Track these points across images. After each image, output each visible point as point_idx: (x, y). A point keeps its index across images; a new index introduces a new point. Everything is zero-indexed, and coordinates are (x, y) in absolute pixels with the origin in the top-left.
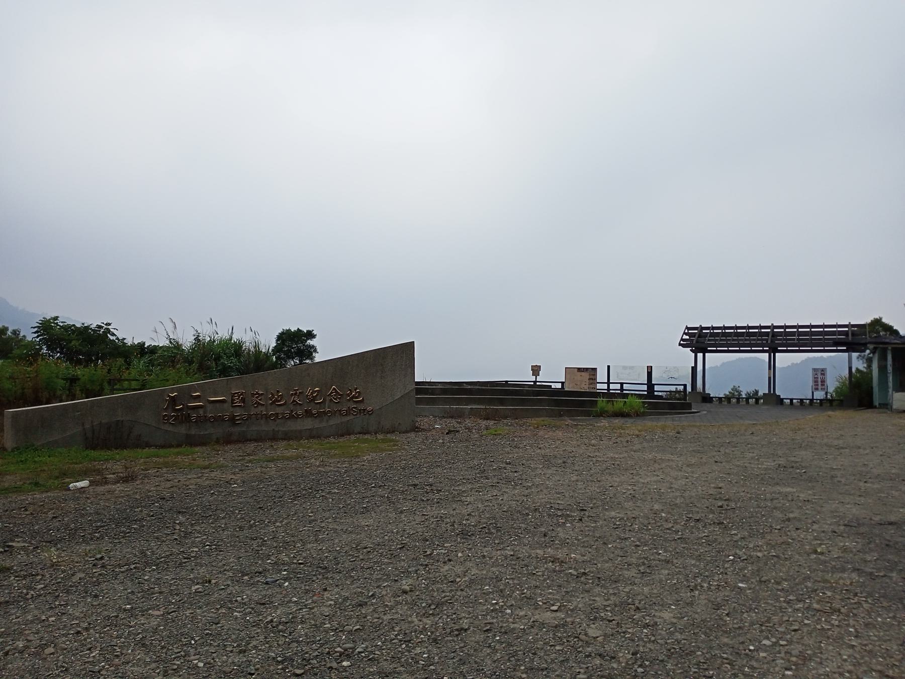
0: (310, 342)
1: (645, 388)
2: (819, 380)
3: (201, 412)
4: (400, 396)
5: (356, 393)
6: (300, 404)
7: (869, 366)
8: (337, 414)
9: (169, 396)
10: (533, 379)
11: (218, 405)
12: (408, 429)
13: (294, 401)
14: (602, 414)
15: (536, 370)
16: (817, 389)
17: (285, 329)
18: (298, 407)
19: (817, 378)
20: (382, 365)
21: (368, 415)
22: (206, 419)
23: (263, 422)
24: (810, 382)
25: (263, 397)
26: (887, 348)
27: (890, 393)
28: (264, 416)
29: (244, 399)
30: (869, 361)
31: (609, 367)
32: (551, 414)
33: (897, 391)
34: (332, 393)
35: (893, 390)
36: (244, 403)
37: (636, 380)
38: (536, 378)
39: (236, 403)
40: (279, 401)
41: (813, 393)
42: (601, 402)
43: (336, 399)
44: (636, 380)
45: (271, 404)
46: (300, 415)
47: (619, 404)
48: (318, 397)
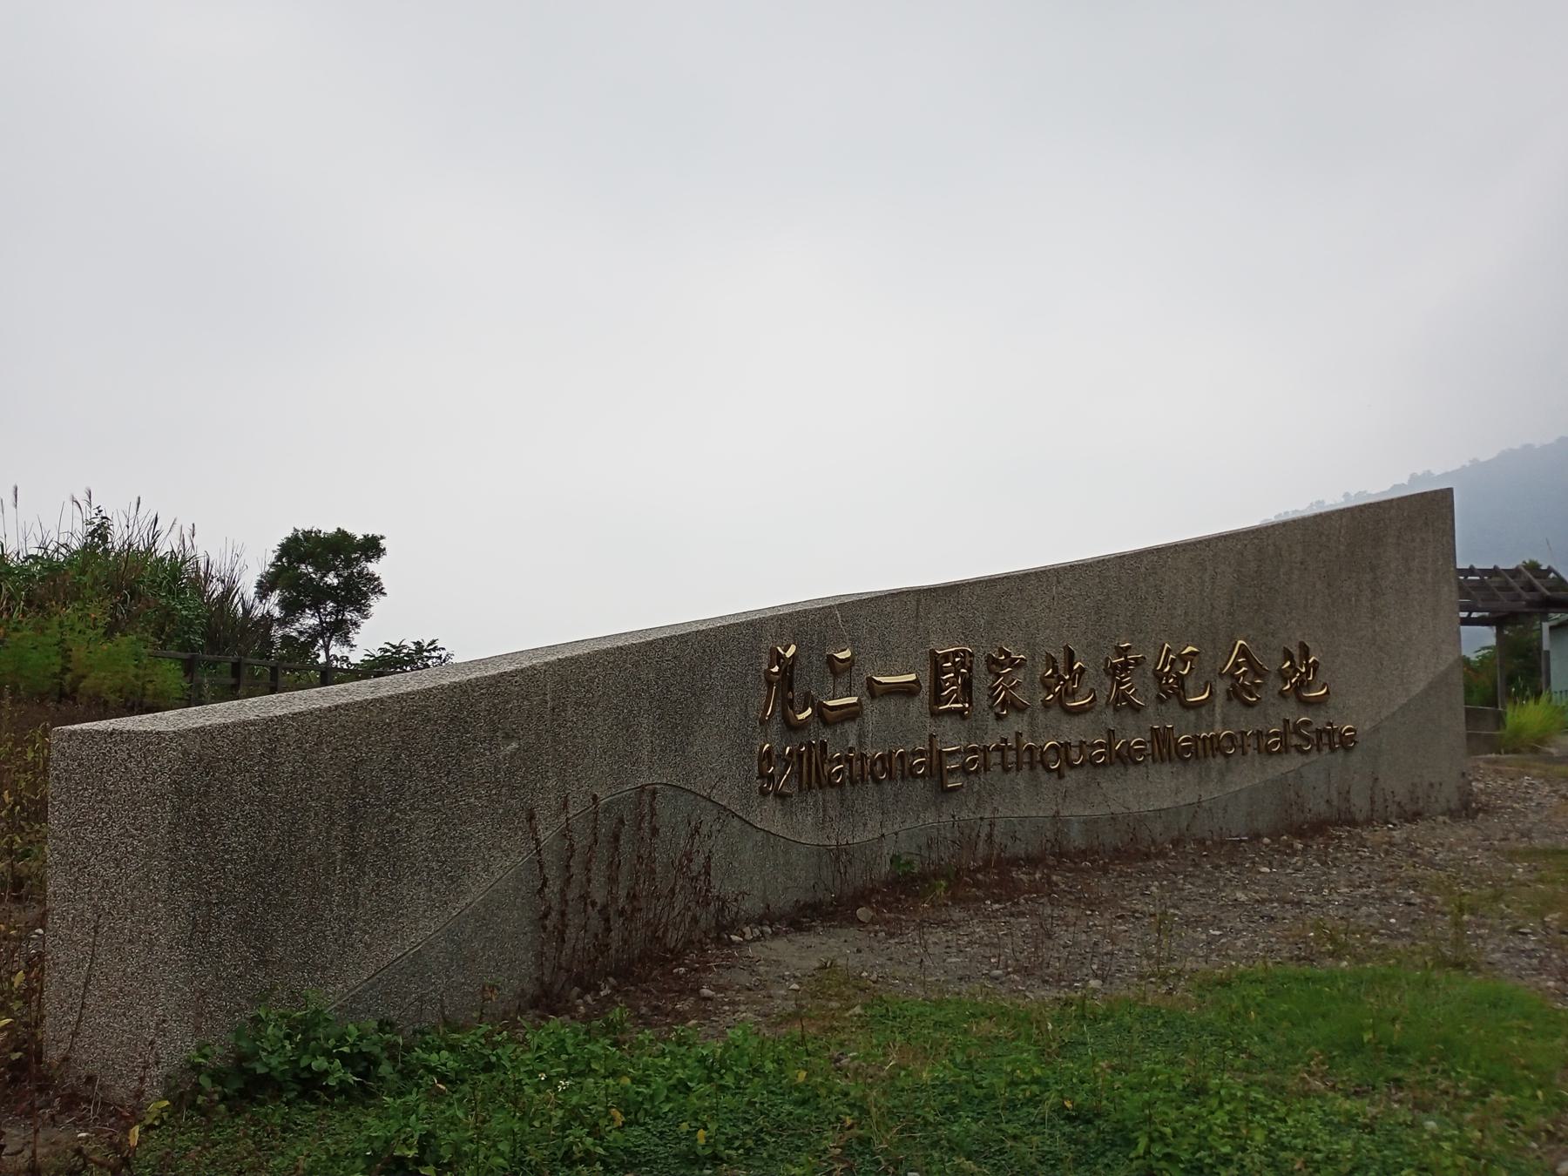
0: (373, 567)
34: (1237, 666)
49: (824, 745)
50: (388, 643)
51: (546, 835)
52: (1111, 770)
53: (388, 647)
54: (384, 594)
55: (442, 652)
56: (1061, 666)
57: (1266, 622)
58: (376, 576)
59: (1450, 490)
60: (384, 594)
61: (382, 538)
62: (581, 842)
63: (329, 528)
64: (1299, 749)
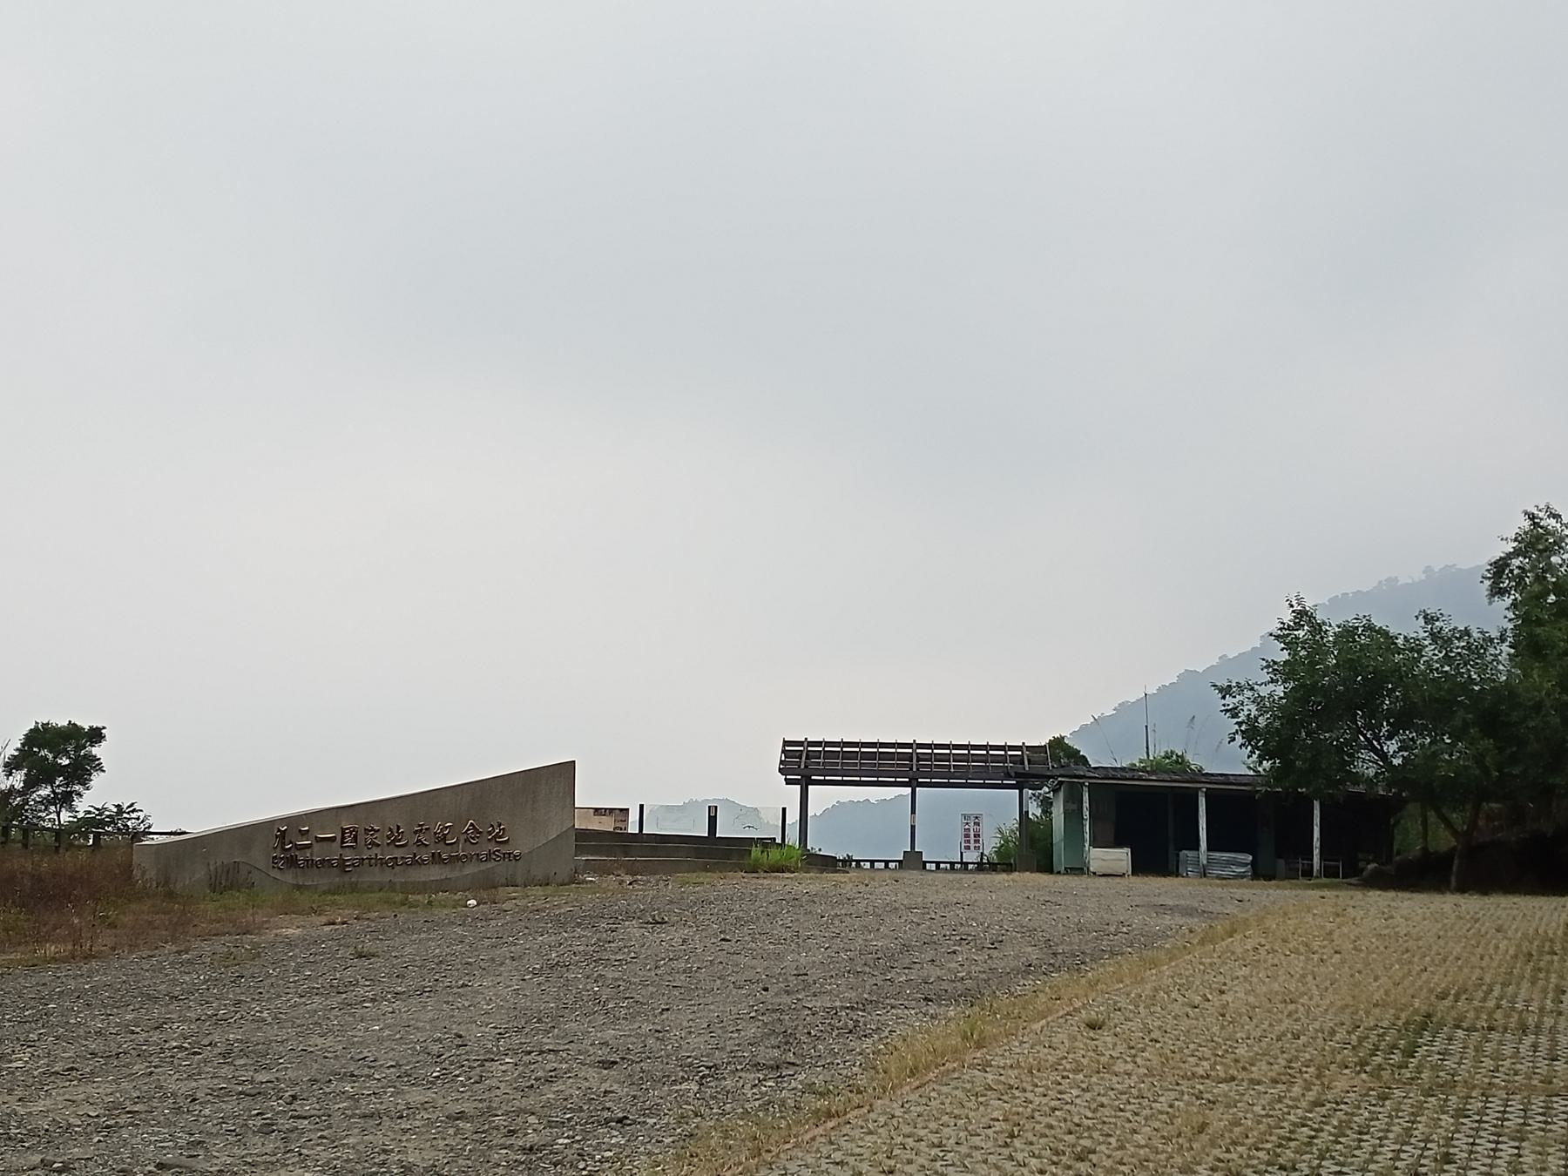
0: (95, 751)
2: (972, 833)
4: (554, 836)
5: (500, 830)
6: (427, 845)
7: (1047, 811)
9: (279, 830)
13: (419, 841)
16: (968, 848)
18: (423, 848)
19: (969, 829)
22: (310, 863)
24: (960, 838)
26: (1084, 783)
27: (1087, 849)
30: (1046, 804)
31: (642, 807)
33: (1095, 843)
34: (468, 830)
35: (1090, 845)
36: (356, 842)
39: (347, 842)
40: (399, 841)
41: (962, 853)
42: (756, 851)
43: (473, 839)
46: (426, 860)
49: (296, 856)
50: (92, 806)
51: (212, 868)
52: (413, 867)
53: (92, 809)
54: (104, 771)
55: (140, 813)
56: (395, 830)
58: (98, 757)
59: (574, 761)
60: (104, 771)
61: (104, 728)
62: (219, 871)
63: (62, 723)
64: (495, 859)
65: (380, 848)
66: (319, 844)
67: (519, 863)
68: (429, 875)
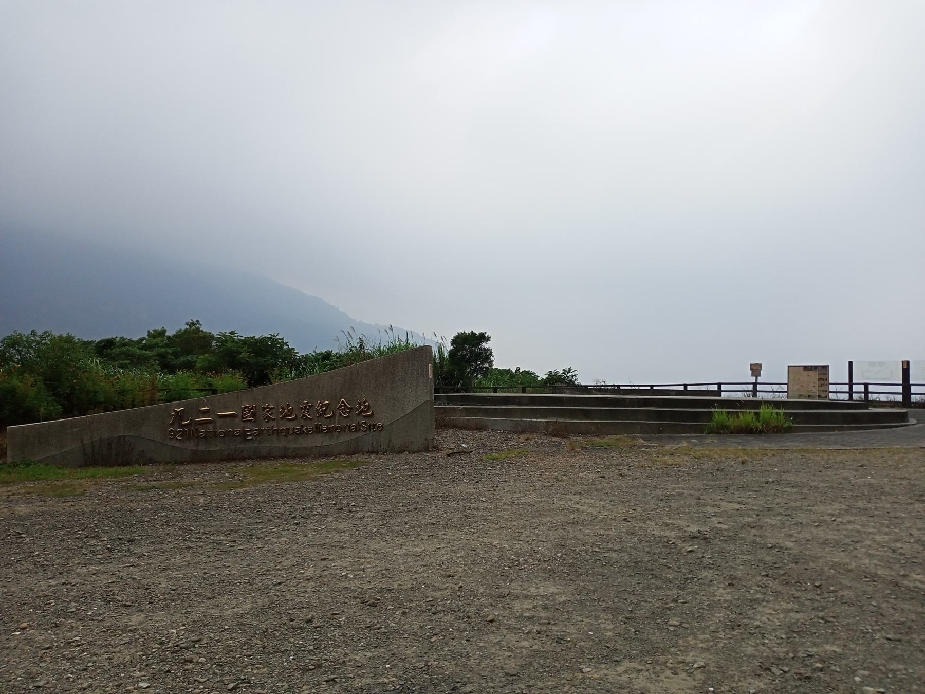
0: (485, 345)
1: (900, 389)
3: (211, 427)
4: (411, 410)
6: (311, 419)
8: (347, 430)
10: (753, 380)
11: (228, 420)
12: (421, 449)
14: (722, 430)
15: (756, 369)
17: (460, 332)
20: (392, 374)
21: (377, 432)
23: (274, 438)
25: (274, 411)
28: (275, 432)
29: (256, 413)
31: (851, 364)
32: (646, 430)
34: (341, 406)
37: (888, 379)
38: (757, 380)
39: (246, 418)
44: (888, 379)
45: (282, 418)
46: (310, 431)
47: (747, 417)
48: (328, 411)
57: (353, 393)
65: (276, 421)
66: (222, 420)
67: (382, 433)
68: (314, 442)
